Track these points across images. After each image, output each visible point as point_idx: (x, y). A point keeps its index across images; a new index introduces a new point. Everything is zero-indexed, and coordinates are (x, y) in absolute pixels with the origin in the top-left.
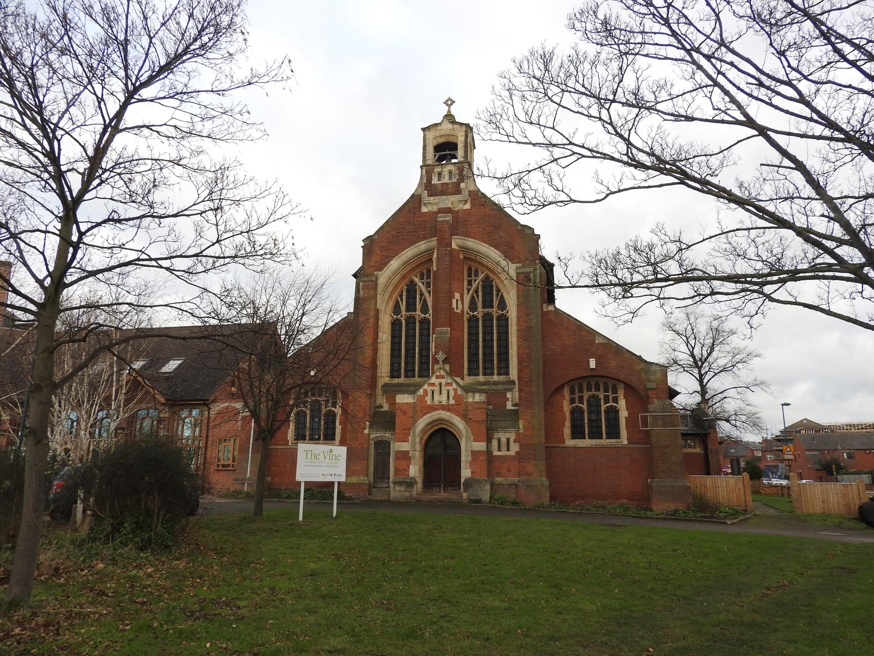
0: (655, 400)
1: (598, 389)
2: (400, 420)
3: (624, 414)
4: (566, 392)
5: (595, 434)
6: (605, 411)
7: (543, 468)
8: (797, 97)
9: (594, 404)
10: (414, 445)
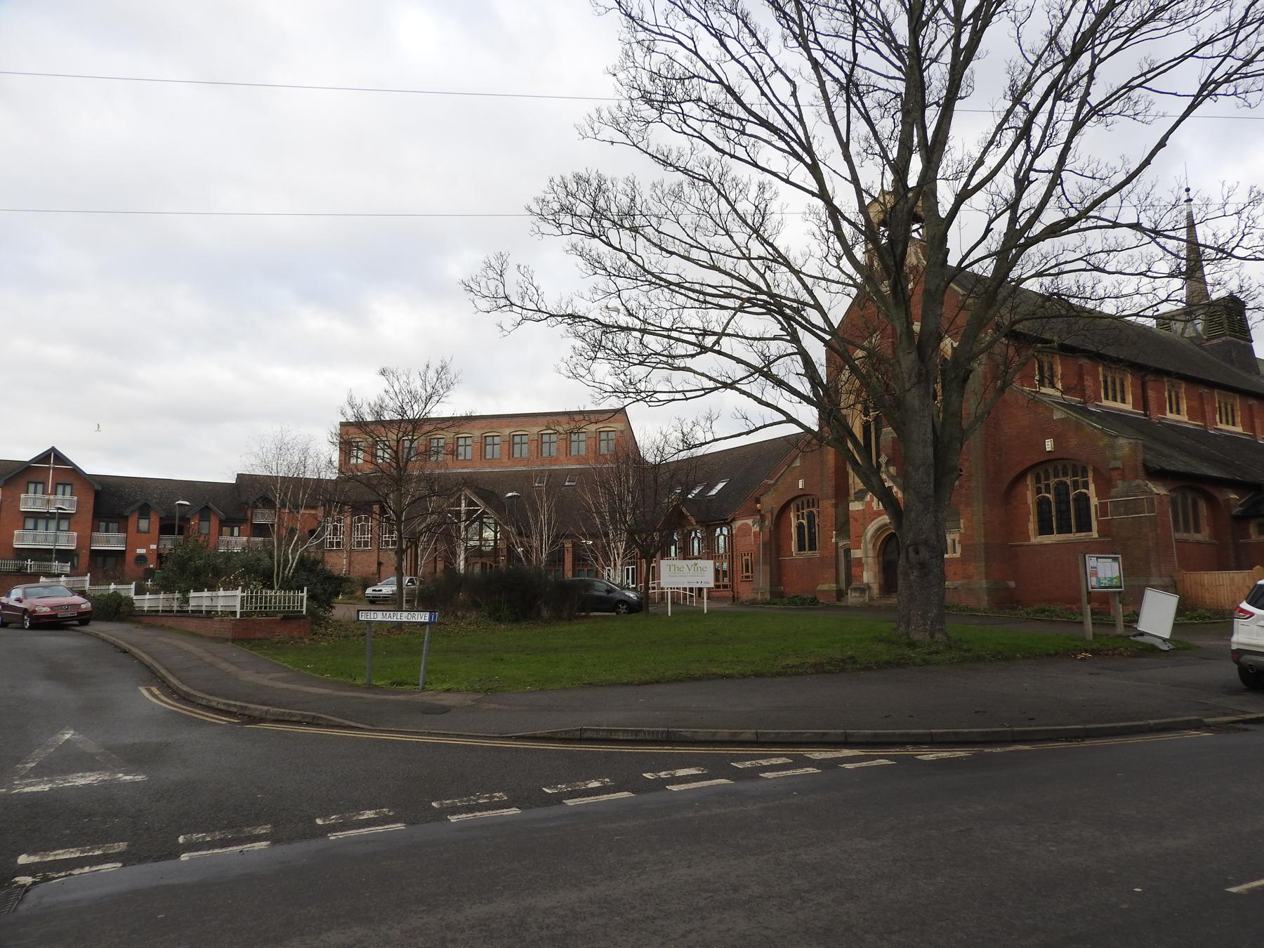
0: (1120, 483)
1: (1065, 475)
2: (853, 526)
3: (1094, 501)
4: (1030, 481)
5: (1064, 528)
6: (1075, 500)
7: (983, 569)
8: (784, 418)
9: (1061, 491)
10: (866, 552)
